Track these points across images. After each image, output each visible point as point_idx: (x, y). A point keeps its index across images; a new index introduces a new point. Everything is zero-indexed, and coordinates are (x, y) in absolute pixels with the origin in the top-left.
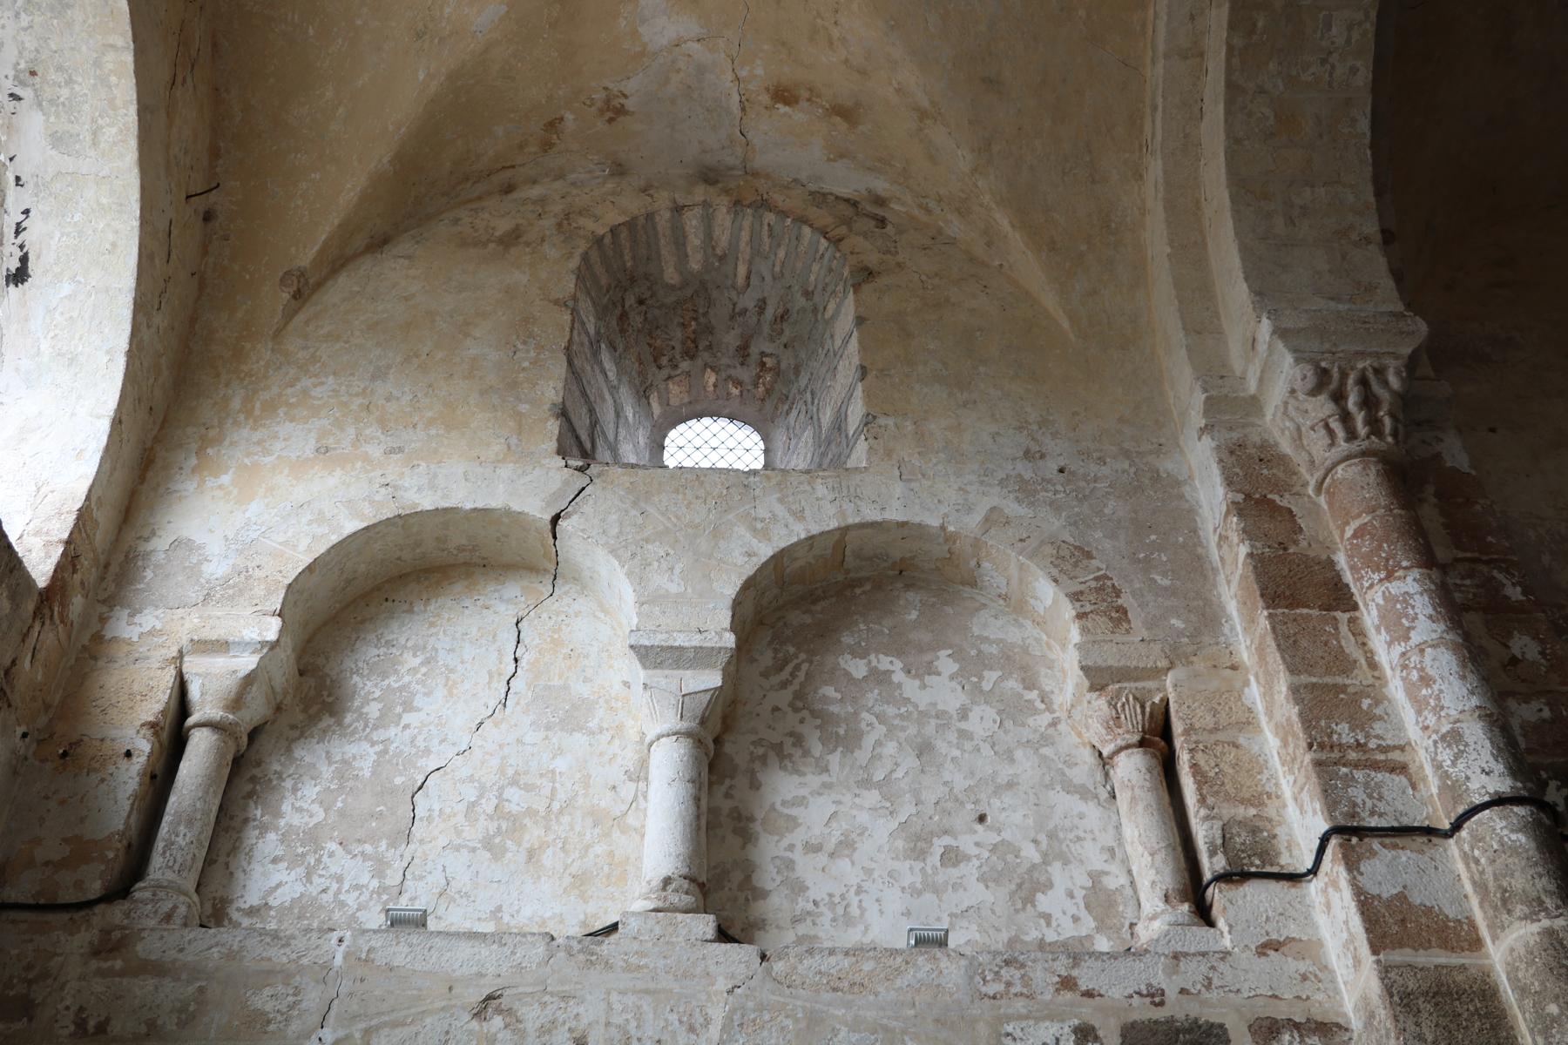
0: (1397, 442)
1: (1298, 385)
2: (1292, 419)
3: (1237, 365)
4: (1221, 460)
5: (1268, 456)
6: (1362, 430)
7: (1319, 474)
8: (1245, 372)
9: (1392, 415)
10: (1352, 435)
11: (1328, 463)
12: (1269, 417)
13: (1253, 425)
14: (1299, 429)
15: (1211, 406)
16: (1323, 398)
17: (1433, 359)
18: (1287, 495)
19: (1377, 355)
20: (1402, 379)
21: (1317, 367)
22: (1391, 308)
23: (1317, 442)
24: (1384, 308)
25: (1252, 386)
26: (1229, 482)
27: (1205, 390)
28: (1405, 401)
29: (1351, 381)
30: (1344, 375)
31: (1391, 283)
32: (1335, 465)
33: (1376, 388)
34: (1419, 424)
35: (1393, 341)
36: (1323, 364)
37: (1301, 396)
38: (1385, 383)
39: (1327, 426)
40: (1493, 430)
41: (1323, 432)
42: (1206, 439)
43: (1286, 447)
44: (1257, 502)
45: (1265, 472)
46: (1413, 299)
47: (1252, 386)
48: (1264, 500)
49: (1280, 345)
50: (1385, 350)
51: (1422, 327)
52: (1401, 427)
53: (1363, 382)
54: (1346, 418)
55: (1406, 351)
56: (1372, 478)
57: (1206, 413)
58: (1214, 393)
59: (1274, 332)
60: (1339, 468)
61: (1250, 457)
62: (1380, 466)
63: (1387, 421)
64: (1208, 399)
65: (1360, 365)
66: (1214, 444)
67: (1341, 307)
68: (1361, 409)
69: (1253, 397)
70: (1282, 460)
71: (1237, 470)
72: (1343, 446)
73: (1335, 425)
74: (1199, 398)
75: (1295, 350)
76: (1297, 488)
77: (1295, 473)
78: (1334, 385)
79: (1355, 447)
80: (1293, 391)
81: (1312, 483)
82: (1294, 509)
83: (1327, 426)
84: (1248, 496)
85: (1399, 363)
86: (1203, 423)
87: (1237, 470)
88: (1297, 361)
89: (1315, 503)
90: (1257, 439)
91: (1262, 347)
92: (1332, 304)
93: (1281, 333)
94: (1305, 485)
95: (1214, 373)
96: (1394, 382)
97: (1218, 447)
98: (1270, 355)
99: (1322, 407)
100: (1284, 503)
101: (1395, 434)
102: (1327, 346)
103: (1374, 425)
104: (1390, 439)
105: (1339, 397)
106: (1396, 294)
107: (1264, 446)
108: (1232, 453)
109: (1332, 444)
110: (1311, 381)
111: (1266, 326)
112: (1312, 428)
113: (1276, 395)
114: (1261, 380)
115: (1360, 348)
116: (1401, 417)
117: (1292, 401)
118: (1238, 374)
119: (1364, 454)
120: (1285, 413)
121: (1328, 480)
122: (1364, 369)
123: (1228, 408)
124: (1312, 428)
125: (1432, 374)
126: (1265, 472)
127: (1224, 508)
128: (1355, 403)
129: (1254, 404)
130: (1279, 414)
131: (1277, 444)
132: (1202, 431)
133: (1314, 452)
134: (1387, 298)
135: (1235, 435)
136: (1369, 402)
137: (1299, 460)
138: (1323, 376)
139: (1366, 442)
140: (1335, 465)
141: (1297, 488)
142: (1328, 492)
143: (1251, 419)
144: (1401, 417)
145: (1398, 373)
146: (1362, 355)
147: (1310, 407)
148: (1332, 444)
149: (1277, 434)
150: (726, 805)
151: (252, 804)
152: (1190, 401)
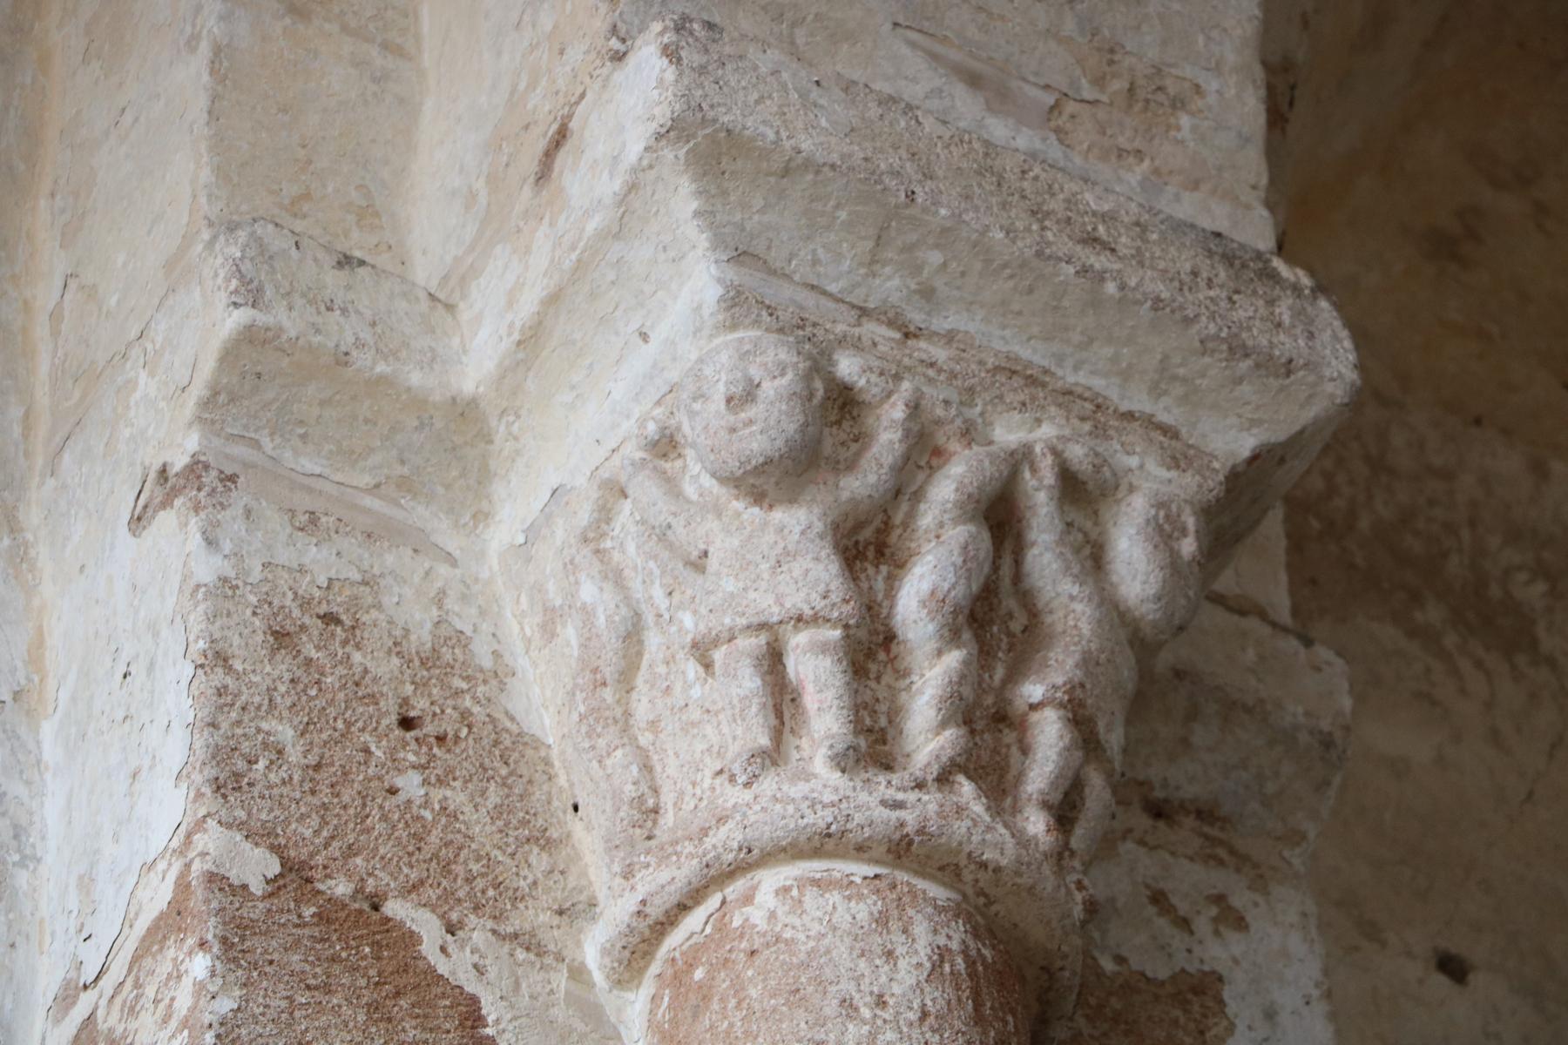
0: (1062, 854)
1: (705, 423)
2: (616, 578)
3: (431, 230)
4: (219, 658)
5: (440, 715)
6: (927, 736)
7: (663, 879)
8: (462, 276)
9: (1080, 720)
10: (873, 745)
11: (725, 839)
12: (503, 532)
13: (421, 545)
14: (632, 637)
15: (253, 378)
16: (798, 523)
17: (1309, 529)
18: (478, 933)
19: (1097, 414)
20: (1174, 566)
21: (818, 364)
22: (1217, 217)
23: (701, 726)
24: (1186, 207)
25: (476, 358)
26: (228, 778)
27: (250, 293)
28: (1154, 680)
29: (946, 489)
30: (923, 451)
31: (1250, 109)
32: (750, 860)
33: (1046, 561)
34: (1159, 811)
35: (1197, 377)
36: (847, 366)
37: (697, 479)
38: (1093, 558)
39: (773, 660)
40: (1453, 967)
41: (749, 682)
42: (177, 538)
43: (541, 698)
44: (330, 915)
45: (411, 784)
46: (1312, 209)
47: (476, 358)
48: (364, 921)
49: (681, 200)
50: (1139, 402)
51: (1336, 362)
52: (1097, 788)
53: (999, 515)
54: (870, 651)
55: (1232, 441)
56: (905, 977)
57: (217, 405)
58: (288, 320)
59: (674, 131)
60: (770, 880)
61: (360, 688)
62: (955, 936)
63: (1049, 742)
64: (250, 337)
65: (1008, 433)
66: (207, 568)
67: (998, 129)
68: (952, 636)
69: (465, 412)
70: (506, 756)
71: (285, 733)
72: (817, 782)
73: (816, 671)
74: (207, 322)
75: (742, 254)
76: (535, 916)
77: (547, 843)
78: (864, 481)
79: (871, 803)
80: (665, 446)
81: (616, 912)
82: (491, 1009)
83: (773, 660)
84: (296, 875)
85: (1186, 485)
86: (183, 446)
87: (285, 733)
88: (738, 305)
89: (593, 1013)
90: (420, 623)
91: (590, 183)
92: (966, 106)
93: (708, 146)
94: (574, 911)
95: (308, 225)
96: (1135, 567)
97: (226, 587)
98: (618, 231)
99: (780, 564)
100: (455, 967)
101: (1065, 809)
102: (890, 286)
103: (987, 727)
104: (1036, 824)
105: (869, 546)
106: (1253, 165)
107: (441, 660)
108: (281, 638)
109: (772, 756)
110: (771, 422)
111: (645, 85)
112: (702, 651)
113: (571, 441)
114: (531, 339)
115: (1033, 353)
116: (1114, 739)
117: (646, 489)
118: (424, 272)
119: (902, 850)
120: (594, 536)
121: (694, 921)
122: (1020, 459)
123: (325, 408)
124: (702, 651)
125: (1280, 600)
126: (411, 784)
127: (158, 895)
128: (935, 601)
129: (456, 445)
130: (562, 531)
131: (500, 675)
132: (168, 485)
133: (670, 771)
134: (1212, 162)
135: (322, 562)
136: (993, 617)
137: (585, 779)
138: (837, 409)
139: (931, 801)
140: (750, 860)
141: (535, 916)
142: (677, 977)
143: (419, 514)
144: (1114, 739)
145: (1163, 532)
146: (1031, 385)
147: (722, 545)
148: (772, 756)
149: (515, 625)
150: (608, 694)
151: (1359, 382)
152: (159, 325)
